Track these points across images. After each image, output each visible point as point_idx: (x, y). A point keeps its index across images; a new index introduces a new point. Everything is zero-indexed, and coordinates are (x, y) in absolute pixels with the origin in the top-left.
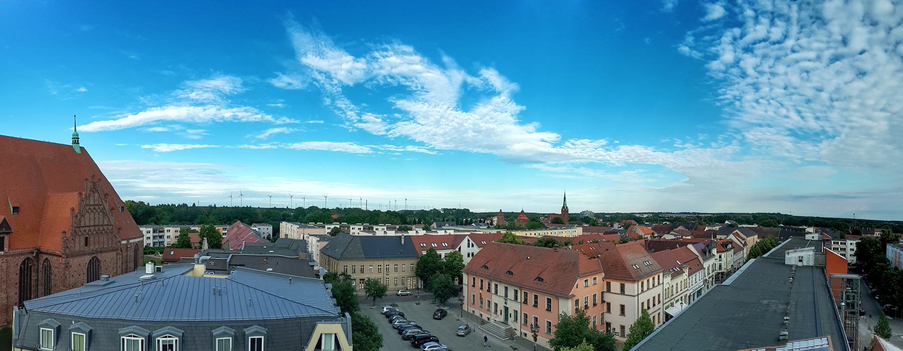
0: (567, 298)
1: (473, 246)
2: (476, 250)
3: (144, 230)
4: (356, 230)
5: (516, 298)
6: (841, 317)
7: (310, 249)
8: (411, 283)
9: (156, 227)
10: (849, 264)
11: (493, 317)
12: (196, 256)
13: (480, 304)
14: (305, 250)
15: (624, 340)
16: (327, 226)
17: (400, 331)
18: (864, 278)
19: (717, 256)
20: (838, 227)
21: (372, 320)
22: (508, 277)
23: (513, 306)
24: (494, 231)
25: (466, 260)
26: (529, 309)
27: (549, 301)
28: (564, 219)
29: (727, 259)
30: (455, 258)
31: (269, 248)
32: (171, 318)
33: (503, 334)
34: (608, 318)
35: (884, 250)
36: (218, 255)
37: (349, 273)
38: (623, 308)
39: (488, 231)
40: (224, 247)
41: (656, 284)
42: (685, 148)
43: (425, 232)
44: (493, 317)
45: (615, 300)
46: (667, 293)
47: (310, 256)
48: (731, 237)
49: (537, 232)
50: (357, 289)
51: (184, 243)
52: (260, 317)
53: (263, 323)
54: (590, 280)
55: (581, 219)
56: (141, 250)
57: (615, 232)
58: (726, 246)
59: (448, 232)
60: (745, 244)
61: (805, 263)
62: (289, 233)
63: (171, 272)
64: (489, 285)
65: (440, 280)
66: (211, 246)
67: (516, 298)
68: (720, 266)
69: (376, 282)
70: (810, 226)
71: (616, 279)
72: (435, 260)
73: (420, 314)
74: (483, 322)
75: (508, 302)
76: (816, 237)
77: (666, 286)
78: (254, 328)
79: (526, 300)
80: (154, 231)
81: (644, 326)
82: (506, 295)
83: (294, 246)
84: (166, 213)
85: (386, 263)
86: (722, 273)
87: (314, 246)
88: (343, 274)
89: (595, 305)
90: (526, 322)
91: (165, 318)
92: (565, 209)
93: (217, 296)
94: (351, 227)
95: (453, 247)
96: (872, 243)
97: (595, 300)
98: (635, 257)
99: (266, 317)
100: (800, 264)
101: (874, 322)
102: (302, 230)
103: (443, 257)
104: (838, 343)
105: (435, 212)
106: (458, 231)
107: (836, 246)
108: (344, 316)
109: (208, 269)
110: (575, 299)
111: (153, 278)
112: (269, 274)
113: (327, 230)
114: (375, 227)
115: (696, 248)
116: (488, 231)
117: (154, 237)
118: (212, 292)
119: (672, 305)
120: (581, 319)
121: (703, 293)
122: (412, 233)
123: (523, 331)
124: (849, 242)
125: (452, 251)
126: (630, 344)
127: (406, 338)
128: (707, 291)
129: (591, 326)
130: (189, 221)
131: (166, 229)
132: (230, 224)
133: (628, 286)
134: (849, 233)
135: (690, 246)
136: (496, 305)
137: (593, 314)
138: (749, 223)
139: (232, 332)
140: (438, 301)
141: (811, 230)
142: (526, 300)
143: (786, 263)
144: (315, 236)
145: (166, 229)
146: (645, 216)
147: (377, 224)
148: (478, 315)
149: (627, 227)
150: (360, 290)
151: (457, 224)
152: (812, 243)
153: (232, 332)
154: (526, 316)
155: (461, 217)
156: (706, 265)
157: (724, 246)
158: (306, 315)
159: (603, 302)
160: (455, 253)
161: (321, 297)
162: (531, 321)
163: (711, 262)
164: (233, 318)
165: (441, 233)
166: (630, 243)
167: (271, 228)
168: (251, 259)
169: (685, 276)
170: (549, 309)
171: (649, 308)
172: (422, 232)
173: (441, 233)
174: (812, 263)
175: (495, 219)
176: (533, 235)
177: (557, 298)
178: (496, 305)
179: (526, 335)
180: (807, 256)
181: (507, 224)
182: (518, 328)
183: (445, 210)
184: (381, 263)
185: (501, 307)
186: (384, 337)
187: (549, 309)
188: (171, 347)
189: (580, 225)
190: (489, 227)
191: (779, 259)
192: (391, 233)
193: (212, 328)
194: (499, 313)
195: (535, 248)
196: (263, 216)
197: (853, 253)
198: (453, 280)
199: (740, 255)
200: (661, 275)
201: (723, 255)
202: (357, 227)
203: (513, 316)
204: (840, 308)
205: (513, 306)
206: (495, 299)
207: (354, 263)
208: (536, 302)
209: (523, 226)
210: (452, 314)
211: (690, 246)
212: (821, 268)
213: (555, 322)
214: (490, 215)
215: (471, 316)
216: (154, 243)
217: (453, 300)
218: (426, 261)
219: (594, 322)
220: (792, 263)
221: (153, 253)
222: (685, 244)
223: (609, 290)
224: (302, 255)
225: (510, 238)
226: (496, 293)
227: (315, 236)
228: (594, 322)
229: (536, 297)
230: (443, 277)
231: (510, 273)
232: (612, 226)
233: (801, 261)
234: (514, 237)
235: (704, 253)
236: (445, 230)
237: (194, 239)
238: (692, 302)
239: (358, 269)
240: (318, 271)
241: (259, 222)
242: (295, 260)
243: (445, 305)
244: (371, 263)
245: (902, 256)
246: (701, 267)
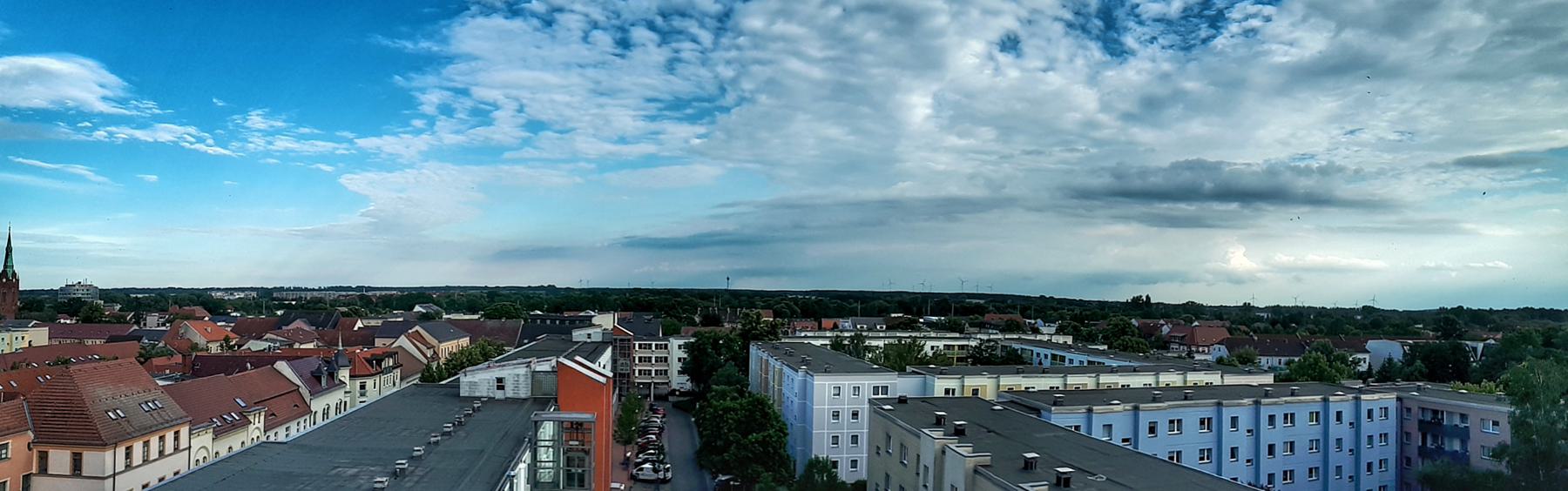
20: (651, 309)
58: (379, 363)
71: (61, 443)
100: (499, 395)
115: (295, 370)
133: (90, 458)
135: (282, 366)
146: (237, 296)
156: (318, 405)
174: (524, 392)
189: (44, 321)
200: (184, 431)
201: (369, 383)
211: (282, 366)
220: (482, 392)
223: (43, 470)
233: (501, 388)
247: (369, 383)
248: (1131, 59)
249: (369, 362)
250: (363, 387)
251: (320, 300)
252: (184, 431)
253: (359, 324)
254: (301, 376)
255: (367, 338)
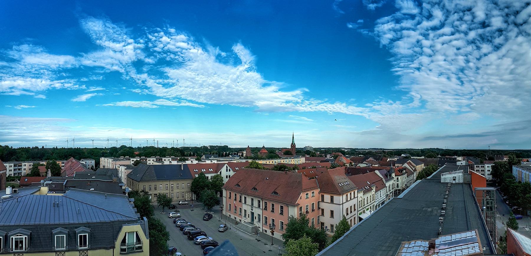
0: (294, 205)
1: (230, 170)
2: (232, 173)
3: (7, 165)
4: (151, 161)
5: (259, 206)
6: (483, 216)
7: (120, 175)
8: (188, 196)
9: (17, 163)
10: (487, 180)
11: (243, 219)
12: (42, 181)
13: (234, 211)
14: (117, 175)
15: (332, 234)
16: (132, 159)
17: (182, 228)
18: (498, 190)
19: (395, 178)
21: (161, 221)
22: (253, 191)
23: (257, 212)
24: (244, 161)
25: (225, 180)
26: (268, 214)
27: (282, 207)
28: (293, 151)
29: (402, 180)
30: (218, 179)
31: (92, 175)
32: (22, 223)
33: (250, 230)
34: (322, 219)
35: (511, 170)
36: (58, 180)
37: (147, 190)
38: (332, 212)
39: (240, 161)
40: (63, 175)
41: (352, 197)
42: (380, 104)
43: (197, 162)
44: (243, 219)
45: (327, 207)
46: (358, 204)
47: (120, 179)
48: (406, 165)
49: (274, 161)
50: (153, 201)
51: (35, 173)
52: (85, 221)
53: (88, 225)
54: (310, 193)
55: (304, 152)
56: (4, 179)
57: (327, 161)
59: (213, 161)
60: (415, 170)
61: (457, 181)
62: (106, 165)
63: (25, 193)
64: (241, 197)
65: (207, 194)
66: (54, 174)
67: (259, 206)
68: (398, 185)
69: (164, 196)
70: (459, 156)
71: (328, 193)
72: (203, 180)
73: (194, 217)
74: (237, 223)
75: (254, 209)
76: (464, 163)
77: (360, 199)
78: (59, 230)
79: (266, 207)
80: (15, 166)
81: (344, 226)
82: (252, 204)
83: (109, 173)
84: (24, 153)
85: (172, 183)
86: (399, 190)
87: (123, 173)
88: (143, 191)
89: (313, 210)
90: (266, 222)
91: (17, 223)
92: (293, 145)
93: (56, 207)
94: (148, 159)
95: (216, 172)
96: (502, 165)
97: (313, 207)
98: (340, 178)
99: (89, 221)
100: (454, 182)
101: (506, 220)
102: (114, 162)
103: (209, 178)
104: (482, 234)
105: (205, 149)
106: (220, 161)
107: (478, 169)
108: (142, 219)
109: (50, 190)
110: (300, 206)
111: (11, 197)
112: (92, 192)
113: (131, 162)
114: (163, 159)
115: (381, 173)
116: (240, 161)
117: (15, 170)
118: (52, 205)
119: (364, 212)
120: (304, 220)
121: (386, 203)
122: (188, 162)
123: (264, 228)
124: (486, 165)
125: (215, 174)
126: (335, 238)
127: (185, 233)
128: (388, 201)
129: (310, 224)
130: (39, 158)
131: (23, 164)
132: (67, 160)
133: (336, 198)
134: (486, 160)
136: (245, 211)
137: (311, 217)
138: (418, 156)
139: (88, 230)
140: (206, 208)
141: (460, 158)
142: (266, 207)
143: (442, 181)
144: (124, 165)
145: (23, 164)
147: (165, 157)
148: (233, 218)
149: (336, 157)
150: (154, 201)
151: (219, 156)
152: (461, 167)
153: (66, 231)
154: (266, 218)
155: (222, 151)
156: (387, 184)
157: (400, 172)
158: (116, 219)
159: (319, 208)
160: (217, 176)
161: (125, 207)
162: (270, 222)
163: (391, 183)
164: (67, 222)
165: (208, 162)
166: (338, 168)
167: (93, 162)
168: (81, 183)
169: (373, 192)
170: (282, 213)
171: (347, 214)
172: (195, 162)
173: (208, 162)
174: (461, 181)
175: (245, 152)
176: (271, 163)
177: (287, 206)
178: (245, 211)
179: (266, 231)
180: (459, 176)
181: (253, 155)
182: (261, 226)
183: (211, 146)
184: (168, 183)
185: (249, 212)
186: (171, 234)
187: (282, 213)
188: (21, 242)
189: (303, 156)
190: (240, 158)
191: (437, 179)
192: (175, 163)
193: (52, 229)
194: (247, 216)
195: (274, 172)
196: (88, 154)
197: (489, 173)
198: (216, 193)
199: (411, 177)
200: (356, 191)
201: (399, 178)
202: (151, 159)
203: (257, 218)
204: (482, 210)
205: (257, 212)
206: (244, 207)
207: (150, 183)
208: (273, 209)
209: (264, 156)
210: (216, 217)
212: (468, 184)
213: (286, 222)
214: (241, 150)
215: (228, 218)
216: (14, 174)
217: (217, 207)
218: (198, 181)
219: (313, 222)
220: (448, 181)
221: (13, 180)
222: (373, 170)
223: (323, 200)
224: (115, 179)
225: (255, 165)
226: (245, 202)
227: (124, 165)
228: (313, 222)
229: (273, 205)
230: (209, 192)
231: (255, 189)
232: (326, 157)
233: (454, 180)
234: (258, 164)
235: (386, 176)
236: (211, 160)
237: (42, 170)
238: (378, 208)
239: (153, 188)
240: (125, 190)
241: (86, 158)
242: (109, 184)
243: (211, 211)
244: (160, 183)
245: (526, 174)
246: (385, 186)
247: (399, 178)
248: (402, 78)
249: (399, 171)
250: (398, 179)
251: (371, 152)
252: (356, 191)
253: (388, 160)
254: (382, 175)
255: (389, 164)
